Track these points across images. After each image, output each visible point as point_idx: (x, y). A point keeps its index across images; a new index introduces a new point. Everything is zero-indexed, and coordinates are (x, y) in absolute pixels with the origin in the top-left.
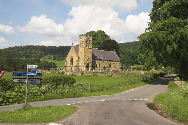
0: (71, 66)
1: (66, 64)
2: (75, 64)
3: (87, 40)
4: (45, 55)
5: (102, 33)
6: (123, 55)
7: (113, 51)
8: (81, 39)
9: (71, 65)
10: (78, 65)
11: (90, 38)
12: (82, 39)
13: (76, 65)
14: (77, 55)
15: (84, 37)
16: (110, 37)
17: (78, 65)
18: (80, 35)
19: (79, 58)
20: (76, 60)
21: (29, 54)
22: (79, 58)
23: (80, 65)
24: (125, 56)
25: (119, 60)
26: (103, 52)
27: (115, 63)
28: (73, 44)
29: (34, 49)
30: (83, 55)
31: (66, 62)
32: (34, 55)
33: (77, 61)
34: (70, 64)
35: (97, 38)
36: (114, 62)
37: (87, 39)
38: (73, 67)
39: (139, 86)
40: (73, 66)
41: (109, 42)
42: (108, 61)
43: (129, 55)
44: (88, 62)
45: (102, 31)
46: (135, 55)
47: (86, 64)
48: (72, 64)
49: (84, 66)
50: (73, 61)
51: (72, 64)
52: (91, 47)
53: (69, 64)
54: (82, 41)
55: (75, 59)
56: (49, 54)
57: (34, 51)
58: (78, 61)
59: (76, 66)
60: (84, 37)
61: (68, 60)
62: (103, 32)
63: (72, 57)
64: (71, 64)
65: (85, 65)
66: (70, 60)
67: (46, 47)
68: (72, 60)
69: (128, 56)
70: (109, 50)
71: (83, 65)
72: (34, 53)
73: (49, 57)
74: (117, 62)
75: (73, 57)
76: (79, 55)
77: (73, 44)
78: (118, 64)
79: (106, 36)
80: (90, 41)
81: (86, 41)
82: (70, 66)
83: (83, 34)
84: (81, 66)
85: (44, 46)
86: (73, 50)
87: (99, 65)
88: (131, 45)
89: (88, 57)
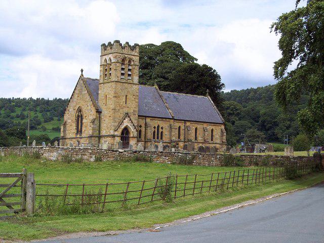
0: (78, 136)
1: (64, 131)
2: (88, 130)
3: (123, 60)
4: (46, 122)
5: (174, 49)
6: (240, 119)
7: (204, 95)
8: (104, 57)
9: (77, 134)
10: (98, 132)
11: (133, 53)
12: (107, 57)
13: (91, 132)
14: (95, 105)
15: (113, 51)
16: (197, 60)
17: (96, 133)
18: (104, 45)
19: (99, 112)
20: (91, 118)
21: (6, 120)
22: (99, 112)
23: (103, 133)
24: (243, 122)
25: (220, 119)
26: (175, 97)
27: (210, 127)
28: (82, 71)
29: (20, 106)
30: (111, 104)
31: (65, 124)
32: (19, 123)
33: (93, 122)
34: (75, 131)
35: (162, 61)
36: (205, 125)
37: (122, 57)
38: (82, 141)
39: (282, 183)
40: (83, 135)
41: (191, 70)
42: (188, 124)
43: (253, 119)
44: (126, 123)
45: (175, 44)
46: (269, 119)
47: (120, 130)
48: (79, 131)
49: (114, 136)
50: (84, 121)
51: (79, 131)
52: (136, 79)
53: (71, 131)
54: (108, 62)
55: (89, 114)
56: (55, 118)
57: (18, 111)
58: (97, 122)
59: (91, 137)
60: (113, 51)
61: (70, 121)
62: (179, 46)
63: (80, 110)
64: (78, 132)
65: (116, 133)
66: (74, 118)
67: (48, 101)
68: (79, 118)
69: (252, 121)
70: (194, 92)
71: (112, 134)
72: (18, 117)
73: (55, 127)
74: (214, 128)
75: (84, 109)
76: (101, 104)
77: (82, 71)
78: (218, 131)
79: (186, 55)
80: (132, 63)
81: (120, 61)
82: (74, 136)
83: (110, 43)
84: (104, 136)
85: (43, 99)
86: (84, 88)
87: (162, 132)
88: (260, 95)
89: (126, 110)
